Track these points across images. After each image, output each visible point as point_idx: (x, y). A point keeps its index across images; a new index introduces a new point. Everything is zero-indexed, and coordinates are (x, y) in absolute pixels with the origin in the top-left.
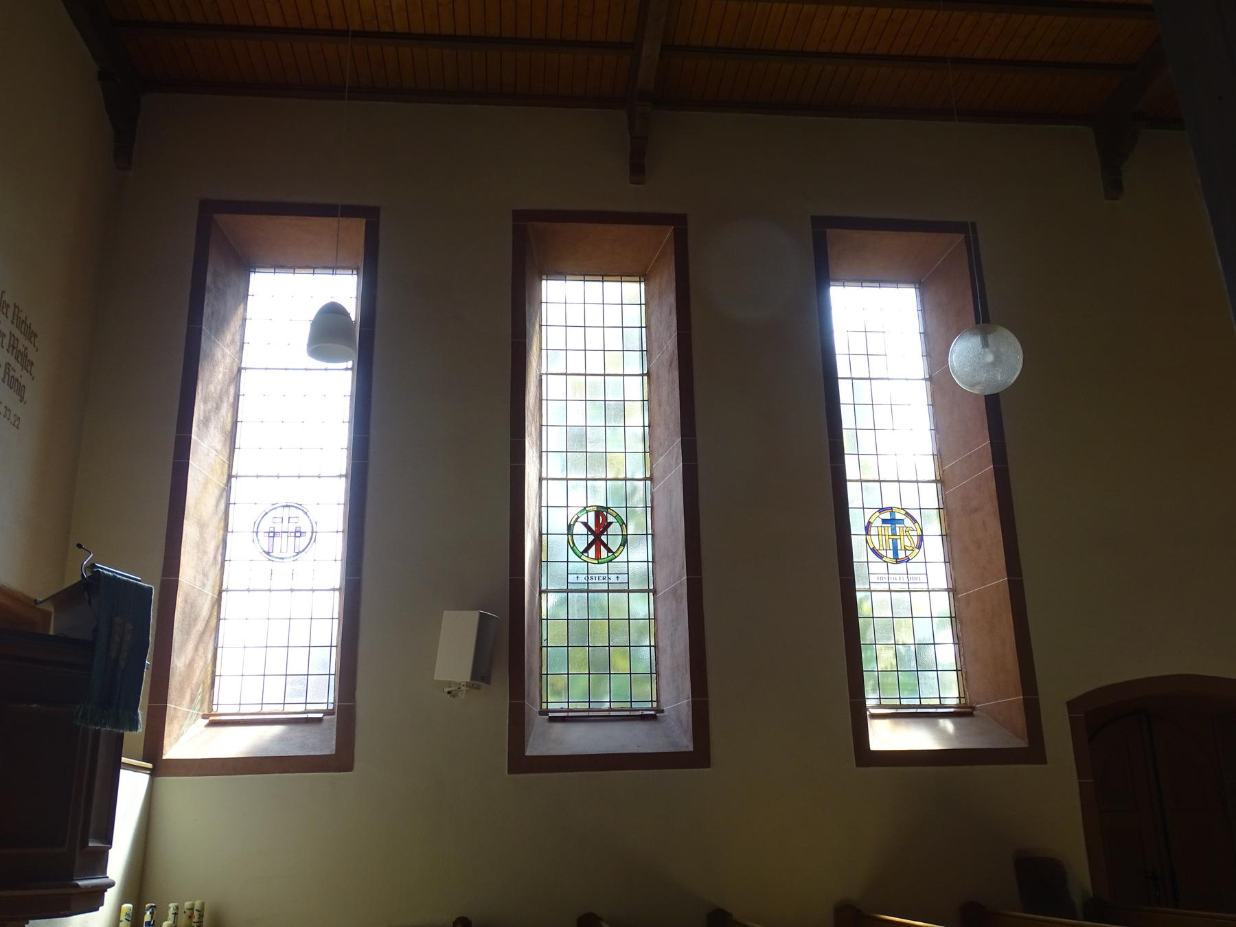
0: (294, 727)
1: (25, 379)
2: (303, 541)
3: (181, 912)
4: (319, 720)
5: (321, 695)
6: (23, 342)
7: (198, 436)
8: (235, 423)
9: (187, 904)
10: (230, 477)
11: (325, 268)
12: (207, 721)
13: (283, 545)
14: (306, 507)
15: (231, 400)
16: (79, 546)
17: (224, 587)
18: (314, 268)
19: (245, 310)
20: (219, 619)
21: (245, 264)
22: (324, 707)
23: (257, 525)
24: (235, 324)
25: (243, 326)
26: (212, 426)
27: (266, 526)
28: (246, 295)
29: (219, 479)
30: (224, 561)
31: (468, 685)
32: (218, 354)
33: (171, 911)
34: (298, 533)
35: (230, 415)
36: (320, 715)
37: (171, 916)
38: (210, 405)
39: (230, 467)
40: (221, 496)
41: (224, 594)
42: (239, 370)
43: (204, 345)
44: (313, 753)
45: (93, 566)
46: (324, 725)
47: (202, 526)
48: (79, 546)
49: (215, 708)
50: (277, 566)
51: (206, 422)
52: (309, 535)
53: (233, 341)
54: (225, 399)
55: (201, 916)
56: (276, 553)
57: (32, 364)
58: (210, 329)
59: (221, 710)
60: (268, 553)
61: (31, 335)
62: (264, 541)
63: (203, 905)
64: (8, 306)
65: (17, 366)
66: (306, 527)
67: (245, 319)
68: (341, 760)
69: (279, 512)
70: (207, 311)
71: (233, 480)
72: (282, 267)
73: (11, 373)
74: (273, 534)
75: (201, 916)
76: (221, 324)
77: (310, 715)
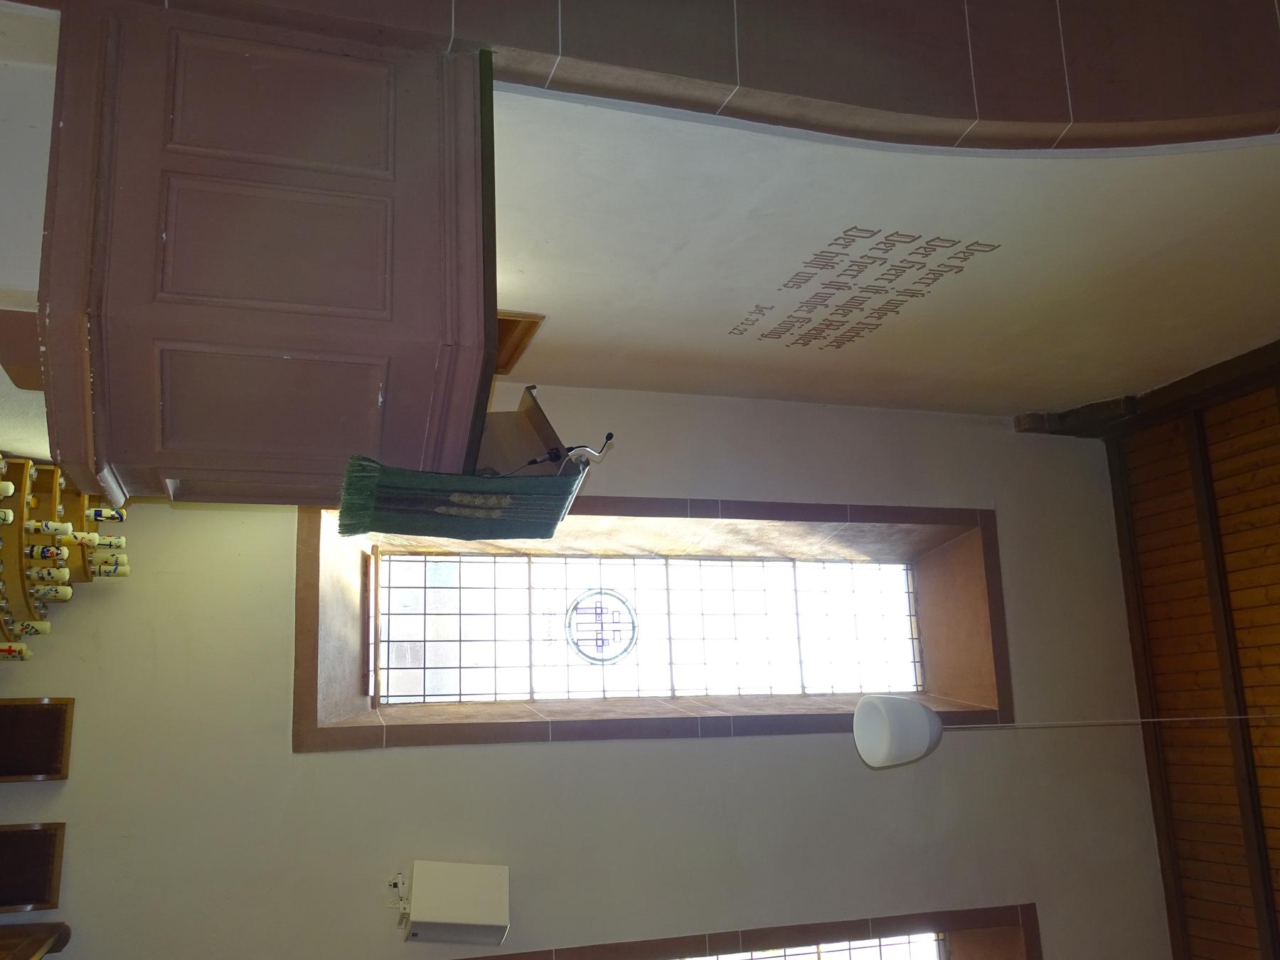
0: (358, 662)
1: (787, 338)
2: (591, 650)
3: (113, 551)
4: (366, 692)
5: (398, 685)
6: (832, 334)
7: (716, 526)
8: (731, 559)
9: (123, 558)
10: (666, 557)
11: (921, 652)
12: (369, 552)
13: (586, 626)
14: (633, 650)
15: (759, 554)
16: (610, 437)
17: (533, 559)
18: (919, 639)
19: (863, 562)
20: (495, 555)
21: (916, 561)
22: (383, 692)
23: (610, 592)
24: (846, 552)
25: (845, 560)
26: (730, 537)
27: (609, 603)
28: (879, 561)
29: (664, 548)
30: (565, 556)
31: (404, 917)
32: (813, 540)
33: (113, 540)
34: (601, 643)
35: (741, 554)
36: (371, 693)
37: (107, 540)
38: (753, 534)
39: (678, 557)
40: (644, 550)
41: (525, 559)
42: (793, 560)
43: (826, 525)
44: (320, 697)
45: (587, 463)
46: (358, 700)
47: (609, 534)
48: (610, 437)
49: (386, 557)
50: (561, 620)
51: (736, 532)
52: (599, 656)
53: (828, 552)
54: (759, 548)
55: (108, 574)
56: (576, 618)
57: (839, 347)
58: (845, 530)
59: (383, 566)
60: (575, 608)
61: (839, 343)
62: (589, 602)
63: (124, 575)
64: (880, 318)
65: (804, 331)
66: (608, 652)
67: (851, 562)
68: (309, 734)
69: (626, 618)
70: (867, 526)
71: (663, 561)
72: (916, 600)
73: (798, 324)
74: (599, 612)
75: (108, 574)
76: (849, 540)
77: (372, 674)
